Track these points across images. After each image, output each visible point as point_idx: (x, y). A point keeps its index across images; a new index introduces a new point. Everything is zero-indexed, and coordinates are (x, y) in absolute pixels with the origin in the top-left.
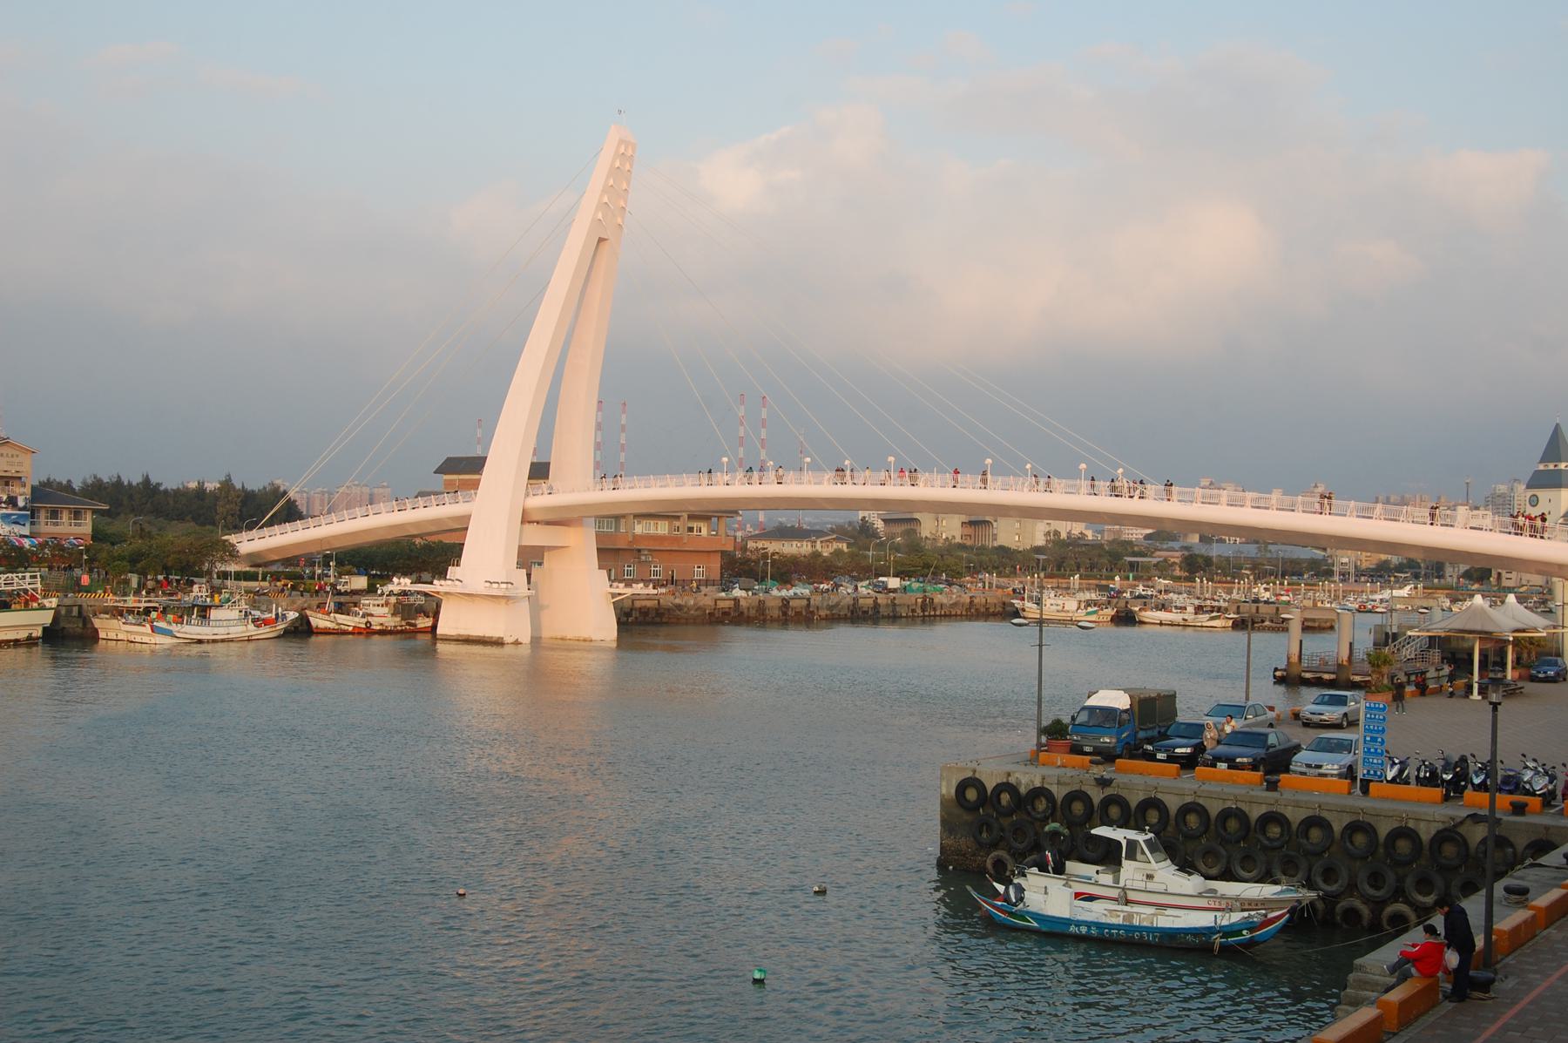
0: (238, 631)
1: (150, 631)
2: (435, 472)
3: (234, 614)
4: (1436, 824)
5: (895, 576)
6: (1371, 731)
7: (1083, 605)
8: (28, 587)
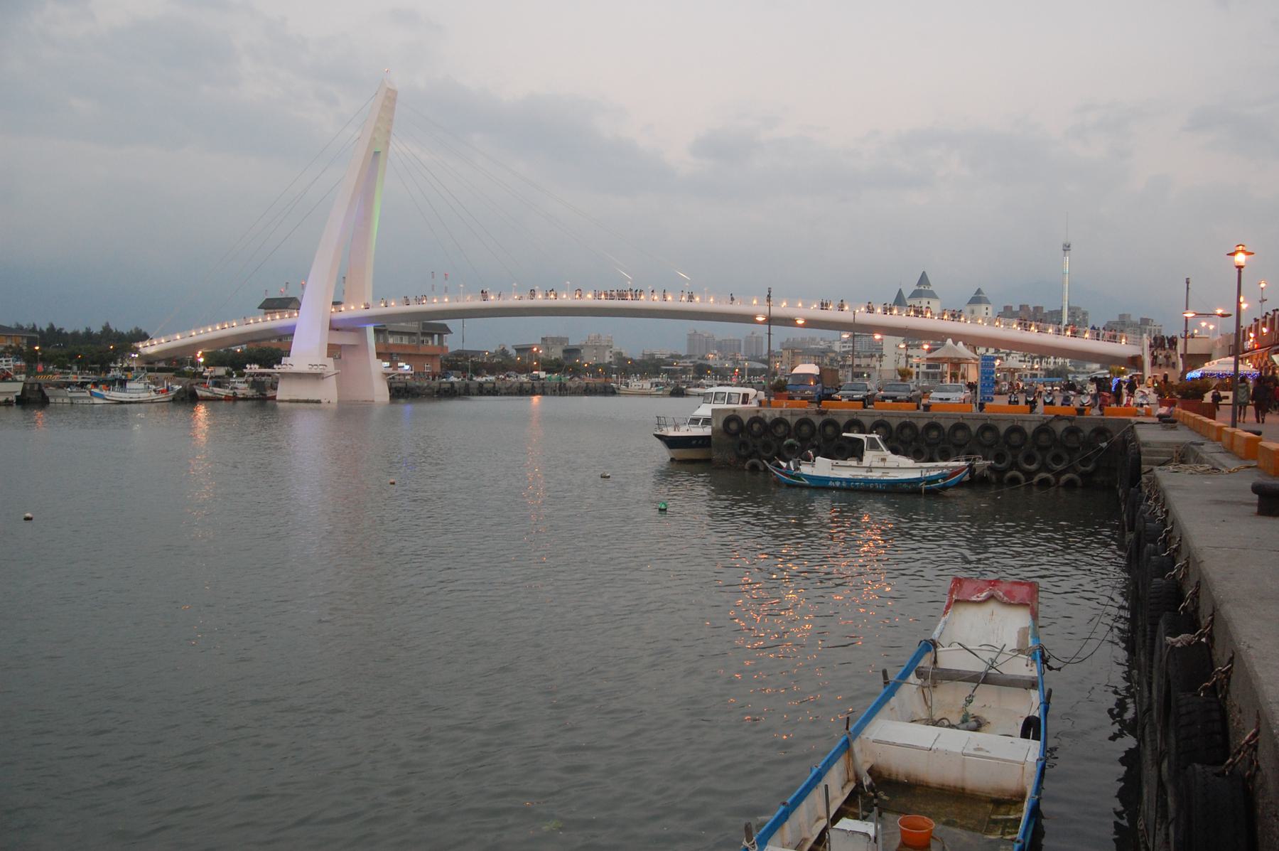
0: (144, 396)
1: (89, 395)
3: (142, 386)
4: (1035, 423)
5: (543, 370)
7: (654, 385)
8: (5, 367)
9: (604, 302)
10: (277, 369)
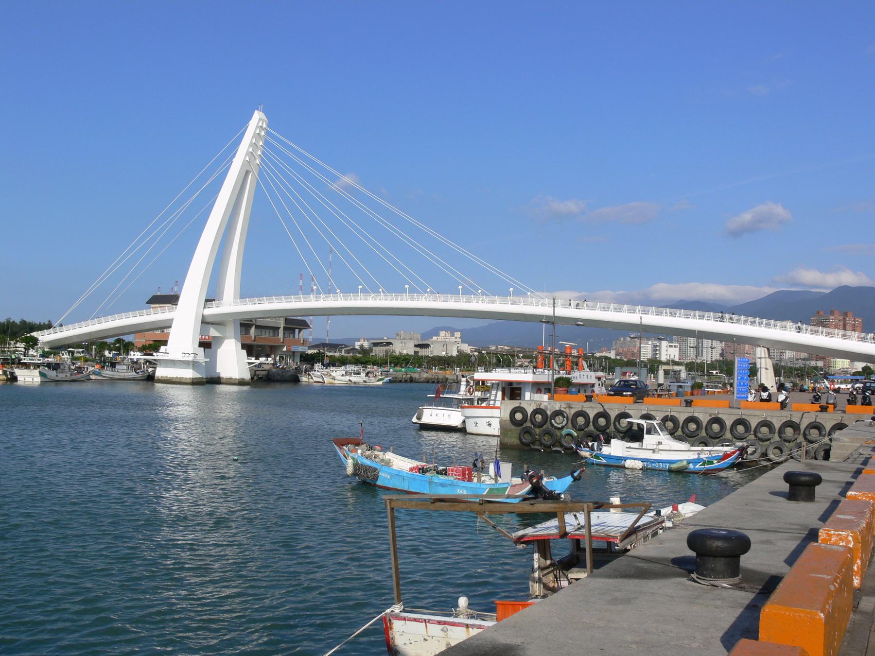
2: (147, 303)
6: (741, 374)
10: (157, 356)
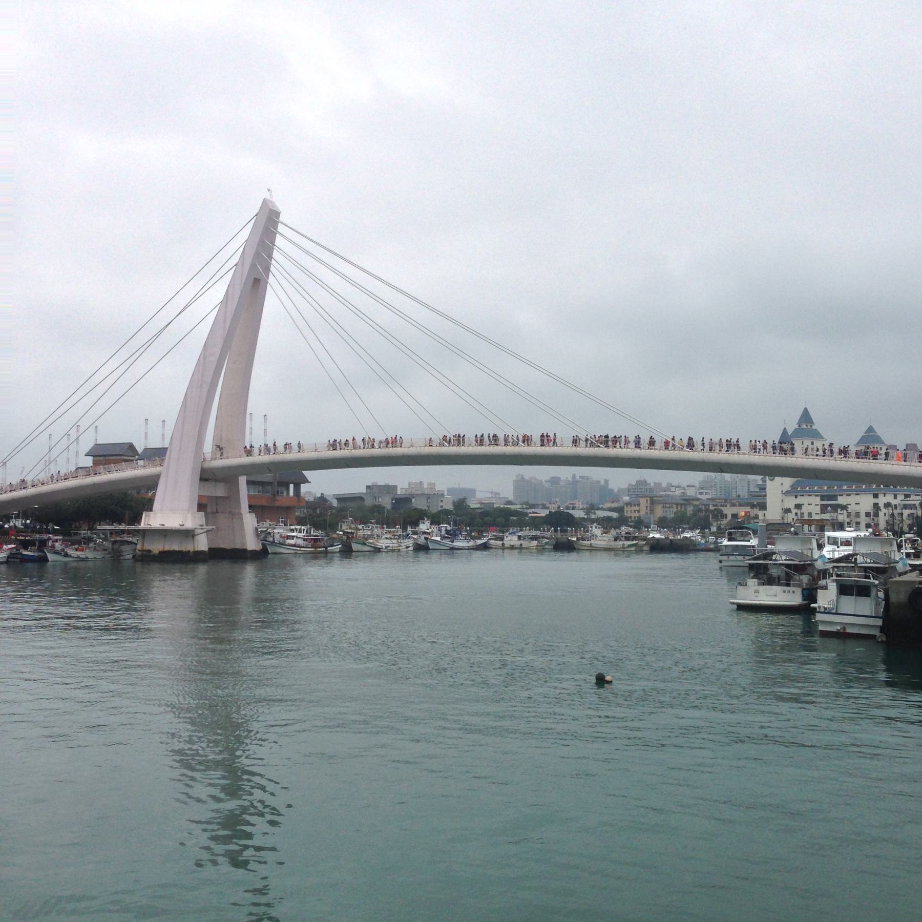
9: (583, 450)
